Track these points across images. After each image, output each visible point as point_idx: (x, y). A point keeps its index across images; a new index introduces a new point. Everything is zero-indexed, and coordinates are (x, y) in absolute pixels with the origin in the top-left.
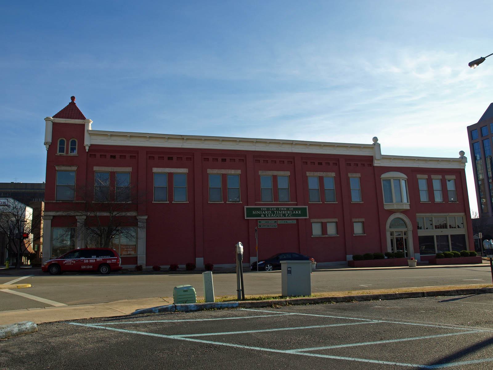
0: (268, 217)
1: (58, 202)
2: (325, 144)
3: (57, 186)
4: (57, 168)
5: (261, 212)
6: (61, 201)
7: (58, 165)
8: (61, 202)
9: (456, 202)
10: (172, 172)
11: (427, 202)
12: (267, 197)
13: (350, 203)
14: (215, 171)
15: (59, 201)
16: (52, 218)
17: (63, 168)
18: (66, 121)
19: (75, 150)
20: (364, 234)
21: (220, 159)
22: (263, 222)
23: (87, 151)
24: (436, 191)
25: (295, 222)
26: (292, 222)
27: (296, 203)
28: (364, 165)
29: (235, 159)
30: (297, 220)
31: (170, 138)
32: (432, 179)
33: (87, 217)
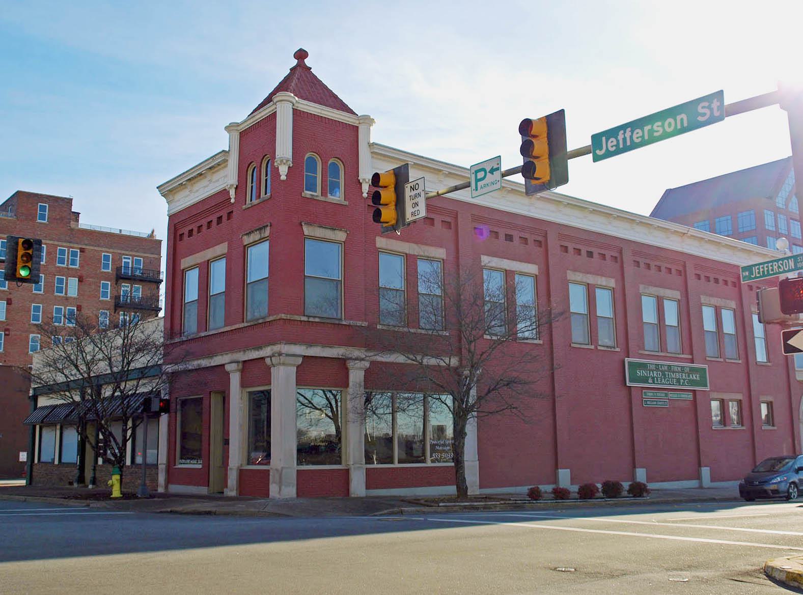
0: (673, 384)
1: (311, 319)
2: (660, 225)
3: (57, 246)
4: (307, 230)
5: (648, 372)
6: (319, 317)
7: (309, 224)
8: (317, 320)
9: (341, 319)
10: (514, 269)
11: (763, 364)
12: (650, 342)
13: (706, 359)
14: (495, 262)
15: (315, 317)
16: (300, 360)
17: (319, 232)
18: (323, 112)
19: (337, 189)
20: (742, 425)
21: (502, 233)
22: (650, 394)
23: (283, 177)
24: (575, 316)
25: (690, 396)
26: (686, 396)
27: (690, 357)
28: (578, 251)
29: (606, 254)
30: (694, 391)
31: (515, 190)
32: (482, 268)
33: (372, 363)
